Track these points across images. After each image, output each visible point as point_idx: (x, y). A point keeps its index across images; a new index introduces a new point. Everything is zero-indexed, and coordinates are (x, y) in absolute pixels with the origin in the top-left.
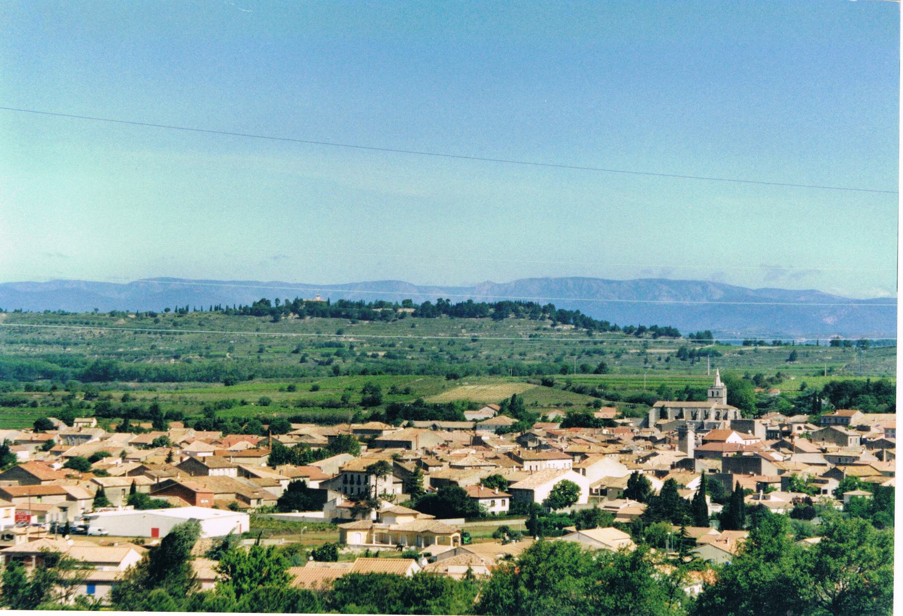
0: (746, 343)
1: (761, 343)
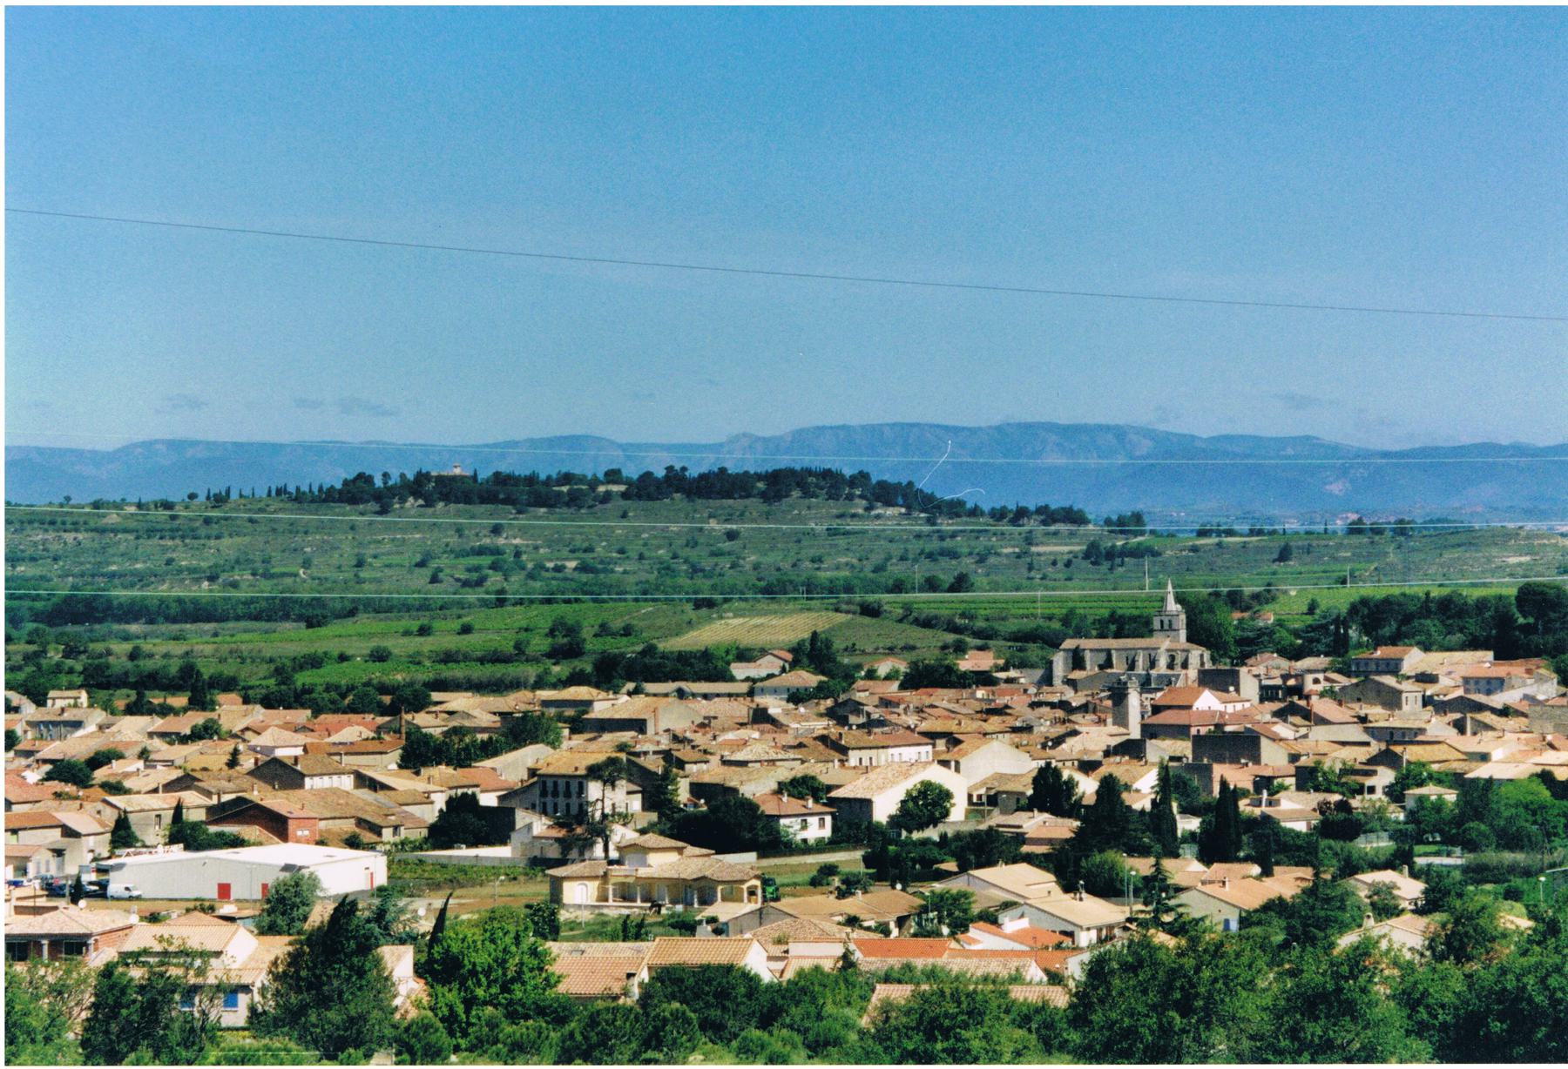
0: (1202, 533)
1: (1230, 533)
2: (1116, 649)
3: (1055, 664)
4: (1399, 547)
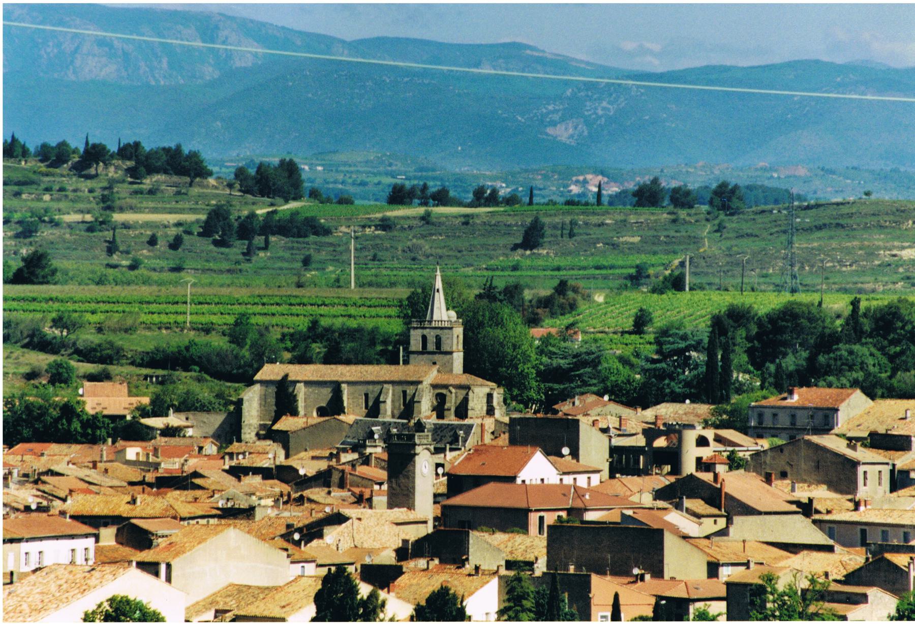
0: (398, 196)
1: (442, 198)
2: (349, 383)
3: (245, 406)
4: (720, 229)
